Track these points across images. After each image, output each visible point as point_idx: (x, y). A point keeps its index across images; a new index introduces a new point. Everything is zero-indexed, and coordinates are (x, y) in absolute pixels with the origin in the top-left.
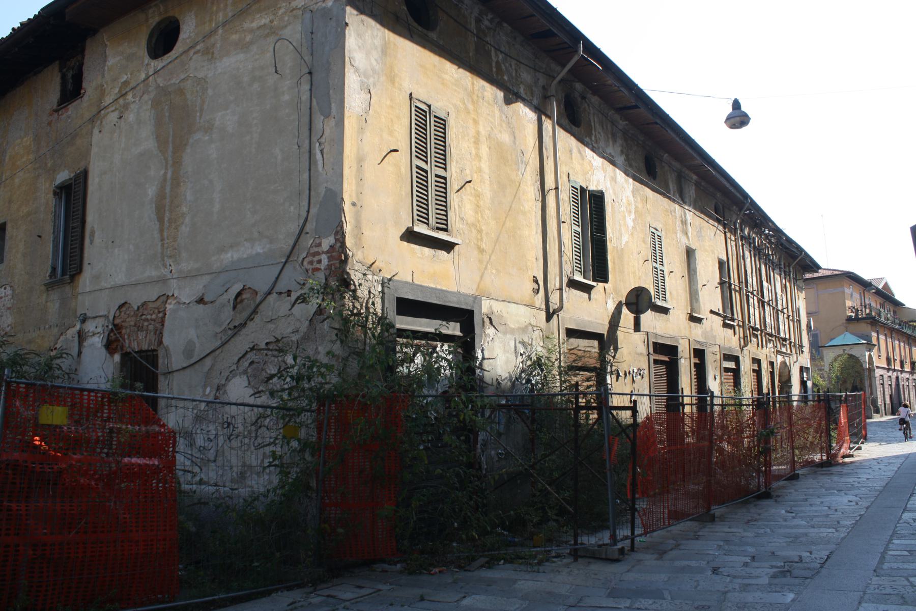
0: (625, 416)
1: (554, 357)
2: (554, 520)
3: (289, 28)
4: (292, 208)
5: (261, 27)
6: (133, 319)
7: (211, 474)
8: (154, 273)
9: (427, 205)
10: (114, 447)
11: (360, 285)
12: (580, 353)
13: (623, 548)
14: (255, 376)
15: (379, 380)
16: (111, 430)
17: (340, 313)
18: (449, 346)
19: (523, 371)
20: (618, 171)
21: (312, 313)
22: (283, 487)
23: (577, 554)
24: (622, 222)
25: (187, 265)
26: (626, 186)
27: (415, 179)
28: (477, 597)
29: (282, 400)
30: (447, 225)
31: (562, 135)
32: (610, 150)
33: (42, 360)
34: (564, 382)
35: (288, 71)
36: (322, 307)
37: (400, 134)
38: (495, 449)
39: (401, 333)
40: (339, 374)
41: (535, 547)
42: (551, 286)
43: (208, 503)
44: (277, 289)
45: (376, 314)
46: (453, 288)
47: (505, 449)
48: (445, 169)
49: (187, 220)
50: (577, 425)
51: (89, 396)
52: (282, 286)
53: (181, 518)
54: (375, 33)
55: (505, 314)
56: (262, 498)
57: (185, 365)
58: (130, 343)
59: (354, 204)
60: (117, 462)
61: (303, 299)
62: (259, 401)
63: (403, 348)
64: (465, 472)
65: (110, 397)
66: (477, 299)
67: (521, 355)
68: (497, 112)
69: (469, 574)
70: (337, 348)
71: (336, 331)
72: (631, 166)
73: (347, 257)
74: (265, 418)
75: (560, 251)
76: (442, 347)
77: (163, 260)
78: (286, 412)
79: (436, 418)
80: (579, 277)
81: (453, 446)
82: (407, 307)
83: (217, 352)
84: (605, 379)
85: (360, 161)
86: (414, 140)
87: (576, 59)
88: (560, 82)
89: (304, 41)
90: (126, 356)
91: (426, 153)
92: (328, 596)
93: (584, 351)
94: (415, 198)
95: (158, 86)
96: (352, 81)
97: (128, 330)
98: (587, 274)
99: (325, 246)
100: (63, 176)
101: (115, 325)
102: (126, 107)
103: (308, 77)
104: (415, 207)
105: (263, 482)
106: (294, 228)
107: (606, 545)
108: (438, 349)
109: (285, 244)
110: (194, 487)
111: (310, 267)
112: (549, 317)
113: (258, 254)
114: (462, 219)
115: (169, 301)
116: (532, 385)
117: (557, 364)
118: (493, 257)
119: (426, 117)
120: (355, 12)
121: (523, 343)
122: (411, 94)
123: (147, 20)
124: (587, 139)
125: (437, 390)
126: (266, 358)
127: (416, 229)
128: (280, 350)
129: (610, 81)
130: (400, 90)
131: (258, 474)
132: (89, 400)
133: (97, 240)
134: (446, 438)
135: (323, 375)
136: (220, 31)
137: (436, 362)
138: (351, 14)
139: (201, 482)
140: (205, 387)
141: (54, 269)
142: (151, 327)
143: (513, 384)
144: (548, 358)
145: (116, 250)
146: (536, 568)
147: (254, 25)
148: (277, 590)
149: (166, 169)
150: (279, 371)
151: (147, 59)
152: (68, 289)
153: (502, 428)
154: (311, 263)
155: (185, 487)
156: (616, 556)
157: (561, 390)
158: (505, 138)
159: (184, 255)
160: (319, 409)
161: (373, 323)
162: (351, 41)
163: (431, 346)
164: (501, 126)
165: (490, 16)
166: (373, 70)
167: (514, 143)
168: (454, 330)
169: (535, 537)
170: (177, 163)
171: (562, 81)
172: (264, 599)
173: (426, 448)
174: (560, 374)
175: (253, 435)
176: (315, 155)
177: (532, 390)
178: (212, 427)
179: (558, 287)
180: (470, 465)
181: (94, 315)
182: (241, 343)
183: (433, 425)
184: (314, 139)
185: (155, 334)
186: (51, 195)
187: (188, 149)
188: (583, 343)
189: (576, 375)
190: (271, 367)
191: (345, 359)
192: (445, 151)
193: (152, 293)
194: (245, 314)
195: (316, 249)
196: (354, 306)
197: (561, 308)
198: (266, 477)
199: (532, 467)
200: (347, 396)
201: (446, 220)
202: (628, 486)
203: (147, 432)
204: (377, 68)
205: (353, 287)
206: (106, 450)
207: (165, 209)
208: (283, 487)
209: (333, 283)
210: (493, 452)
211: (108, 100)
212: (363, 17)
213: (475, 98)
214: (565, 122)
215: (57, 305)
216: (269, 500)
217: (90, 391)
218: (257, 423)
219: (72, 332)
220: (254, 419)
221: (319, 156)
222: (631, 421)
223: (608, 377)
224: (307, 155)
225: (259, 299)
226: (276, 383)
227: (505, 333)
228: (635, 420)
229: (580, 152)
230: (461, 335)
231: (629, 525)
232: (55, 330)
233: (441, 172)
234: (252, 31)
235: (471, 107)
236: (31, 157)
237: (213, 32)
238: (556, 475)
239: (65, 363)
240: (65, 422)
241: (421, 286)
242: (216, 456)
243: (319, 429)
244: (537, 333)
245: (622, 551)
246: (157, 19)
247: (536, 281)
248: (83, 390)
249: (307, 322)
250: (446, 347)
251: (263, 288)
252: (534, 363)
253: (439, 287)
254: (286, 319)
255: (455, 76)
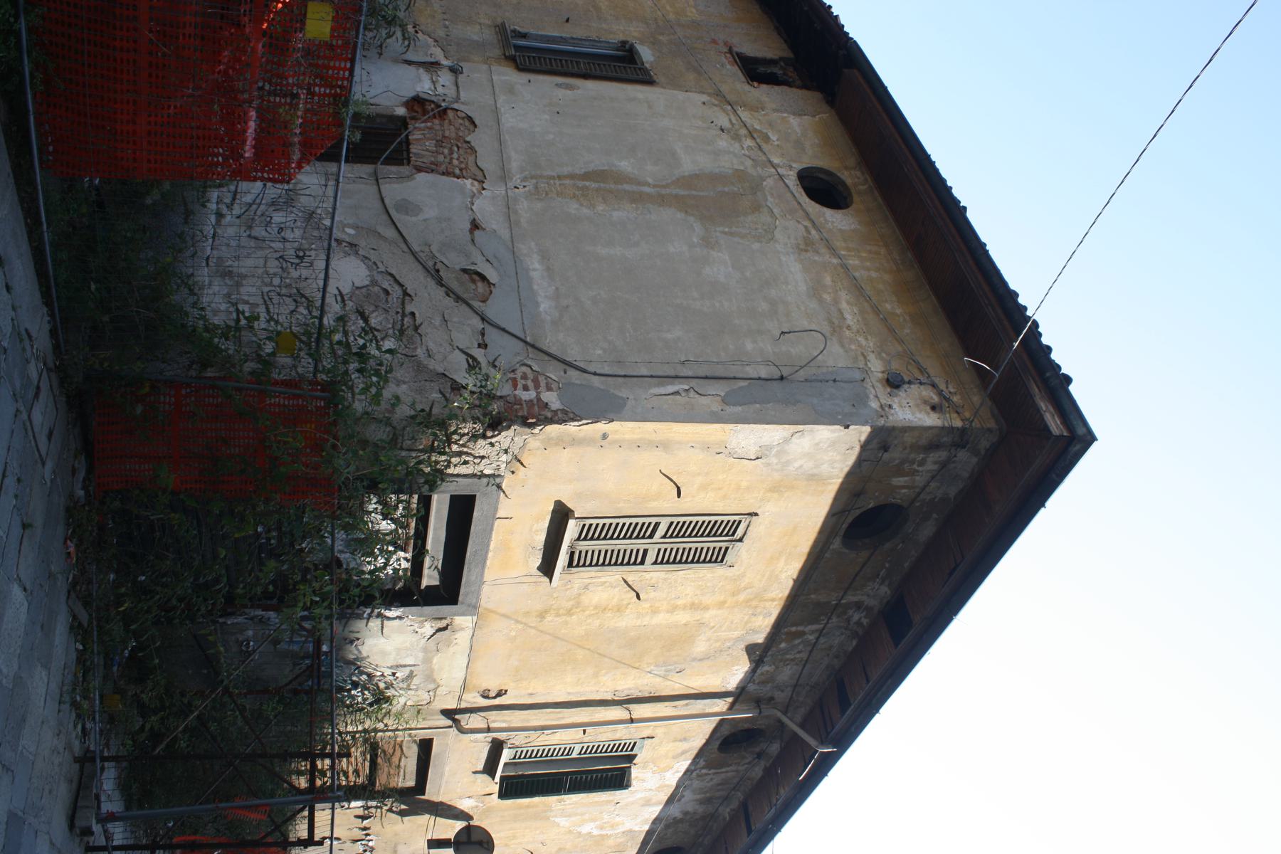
0: (302, 831)
1: (390, 722)
2: (143, 727)
3: (841, 351)
4: (600, 352)
5: (842, 313)
6: (453, 135)
7: (229, 231)
8: (514, 165)
9: (605, 538)
10: (272, 99)
11: (492, 445)
12: (395, 760)
13: (92, 833)
14: (368, 296)
15: (358, 469)
16: (296, 96)
17: (453, 416)
18: (405, 570)
19: (369, 675)
20: (660, 807)
21: (455, 377)
22: (207, 330)
23: (86, 763)
24: (586, 817)
25: (524, 209)
26: (639, 820)
27: (641, 521)
28: (24, 609)
29: (332, 332)
30: (578, 566)
31: (707, 726)
32: (688, 796)
33: (401, 14)
34: (353, 738)
35: (784, 348)
36: (463, 391)
37: (702, 500)
38: (255, 638)
39: (426, 502)
40: (367, 413)
41: (101, 697)
42: (493, 715)
43: (186, 222)
44: (489, 329)
45: (448, 466)
46: (488, 575)
47: (254, 651)
48: (655, 563)
49: (585, 211)
50: (287, 756)
51: (345, 69)
52: (492, 336)
53: (167, 186)
54: (837, 465)
55: (452, 649)
56: (191, 300)
57: (387, 201)
58: (420, 129)
59: (605, 436)
60: (250, 102)
61: (473, 365)
62: (330, 299)
63: (405, 503)
64: (219, 591)
65: (342, 96)
66: (473, 609)
67: (394, 674)
68: (736, 634)
69: (63, 598)
70: (404, 411)
71: (427, 409)
72: (667, 826)
73: (532, 426)
74: (308, 308)
75: (543, 728)
76: (405, 559)
77: (532, 178)
78: (315, 337)
79: (302, 550)
80: (506, 755)
81: (261, 575)
82: (462, 509)
83: (403, 246)
84: (357, 798)
85: (664, 445)
86: (694, 519)
87: (812, 742)
88: (780, 721)
89: (824, 370)
90: (403, 123)
91: (677, 536)
92: (38, 388)
93: (399, 766)
94: (614, 521)
95: (763, 179)
96: (772, 434)
97: (438, 127)
98: (511, 768)
99: (548, 397)
100: (646, 54)
101: (445, 110)
102: (736, 137)
103: (777, 375)
104: (601, 522)
105: (215, 302)
106: (573, 354)
107: (99, 807)
108: (402, 554)
109: (550, 341)
110: (213, 206)
111: (519, 375)
112: (448, 713)
113: (537, 304)
114: (586, 587)
115: (476, 183)
116: (349, 690)
117: (380, 726)
118: (533, 632)
119: (727, 535)
120: (863, 438)
121: (411, 676)
122: (756, 514)
123: (846, 168)
124: (702, 763)
125: (342, 552)
126: (392, 312)
127: (571, 523)
128: (402, 332)
129: (784, 793)
130: (762, 500)
131: (228, 295)
132: (339, 69)
133: (561, 93)
134: (272, 564)
135: (366, 390)
136: (835, 261)
137: (381, 550)
138: (861, 433)
139: (220, 215)
140: (356, 227)
141: (524, 36)
142: (441, 158)
143: (352, 663)
144: (389, 713)
145: (547, 117)
146: (67, 698)
147: (844, 305)
148: (52, 315)
149: (655, 186)
150: (371, 329)
151: (798, 166)
152: (497, 52)
153: (283, 646)
154: (524, 377)
155: (214, 195)
156: (79, 823)
157: (340, 733)
158: (700, 647)
159: (539, 206)
160: (319, 384)
161: (437, 462)
162: (825, 433)
163: (407, 544)
164: (717, 641)
165: (865, 621)
166: (788, 463)
167: (694, 660)
168: (430, 577)
169: (118, 697)
170: (662, 200)
171: (782, 725)
172: (38, 295)
173: (258, 535)
174: (365, 731)
175: (284, 291)
176: (672, 384)
177: (341, 689)
178: (298, 233)
179: (492, 725)
180: (230, 599)
181: (460, 84)
182: (414, 278)
183: (292, 545)
184: (694, 383)
185: (432, 163)
186: (622, 38)
187: (680, 215)
188: (410, 764)
189: (363, 754)
190: (379, 319)
191: (388, 422)
192: (680, 562)
193: (487, 162)
194: (454, 285)
195: (543, 384)
196: (464, 435)
197: (462, 731)
198: (223, 307)
199: (226, 691)
200: (335, 423)
201: (584, 565)
202: (192, 838)
203: (291, 144)
204: (791, 468)
205: (489, 434)
206: (267, 87)
207: (600, 183)
208: (207, 330)
209: (495, 407)
210: (250, 633)
211: (745, 115)
212: (857, 449)
213: (754, 603)
214: (726, 731)
215: (476, 38)
216: (189, 309)
217: (351, 71)
218: (300, 297)
219: (438, 55)
220: (307, 293)
221: (671, 389)
222: (292, 838)
223: (359, 803)
224: (672, 373)
225: (476, 304)
226: (356, 325)
227: (425, 650)
228: (295, 844)
229: (683, 753)
230: (423, 587)
231: (131, 842)
232: (441, 33)
233: (651, 557)
234: (836, 301)
235: (742, 597)
236: (671, 17)
237: (833, 251)
238: (213, 727)
239: (395, 44)
240: (309, 36)
241: (492, 530)
242: (256, 238)
243: (287, 383)
244: (425, 697)
245: (88, 832)
246: (849, 181)
247: (499, 694)
248: (353, 61)
249: (441, 370)
250: (405, 565)
251: (491, 310)
252: (382, 692)
253: (490, 555)
254: (447, 340)
255: (783, 576)
